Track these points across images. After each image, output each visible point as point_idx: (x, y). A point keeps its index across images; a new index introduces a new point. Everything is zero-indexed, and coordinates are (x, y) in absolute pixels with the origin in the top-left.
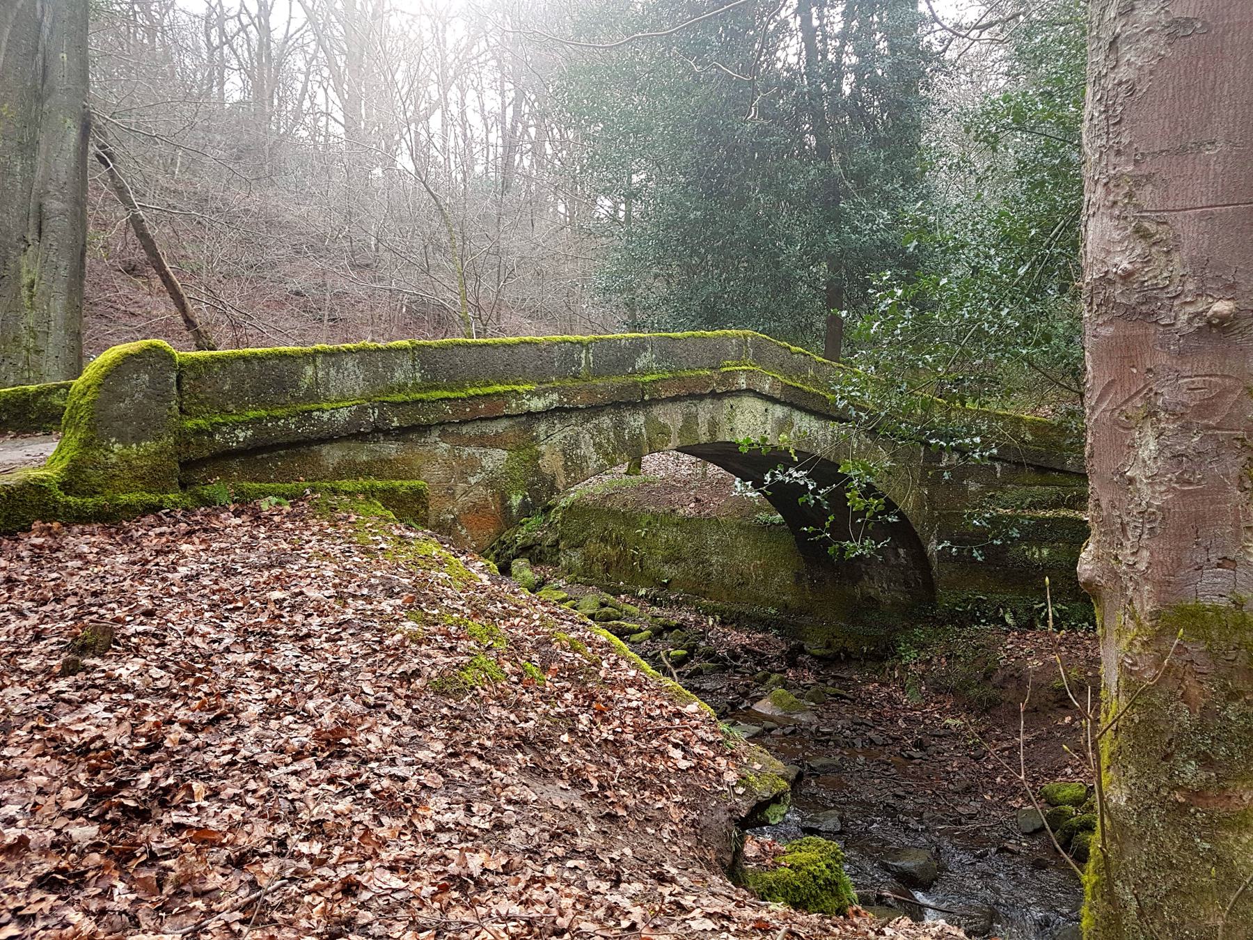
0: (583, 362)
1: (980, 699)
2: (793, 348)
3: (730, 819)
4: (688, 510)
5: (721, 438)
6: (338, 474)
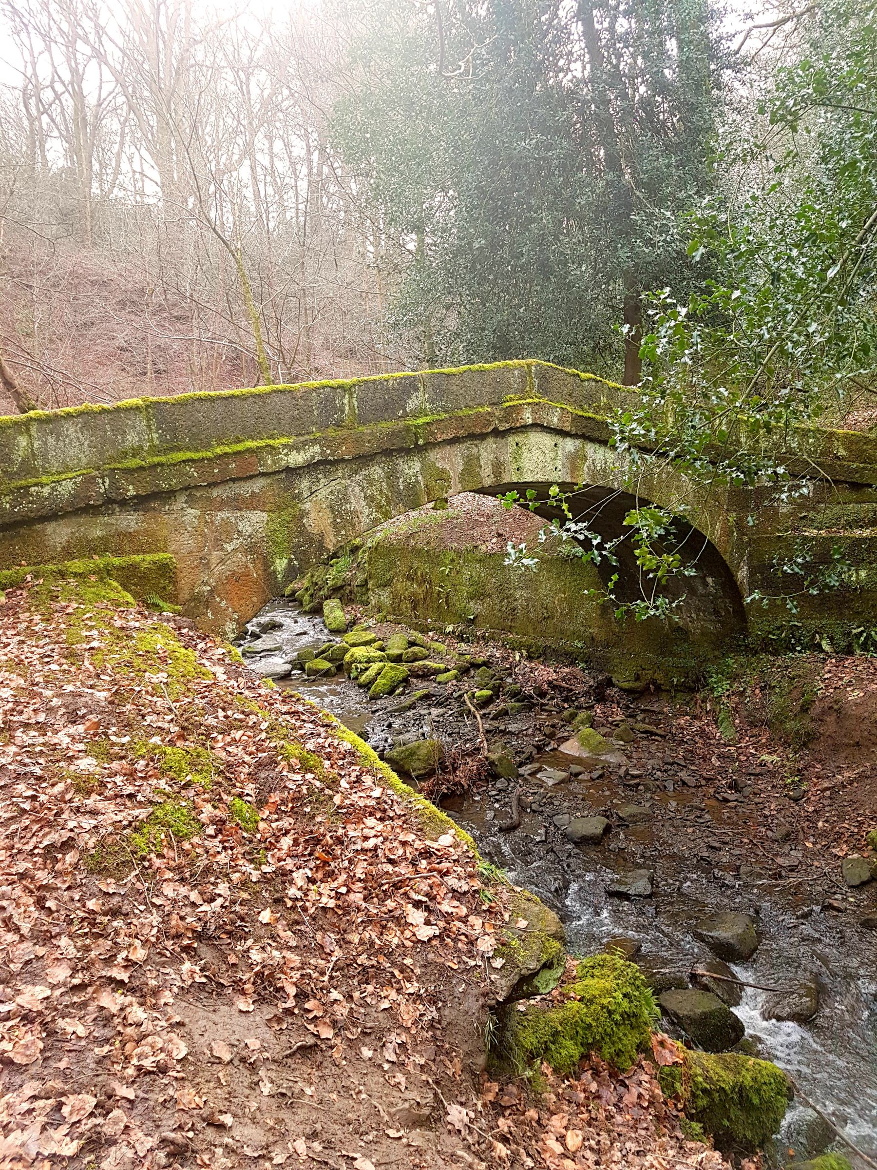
0: (347, 408)
1: (797, 732)
2: (583, 375)
3: (483, 1006)
4: (490, 545)
6: (68, 553)
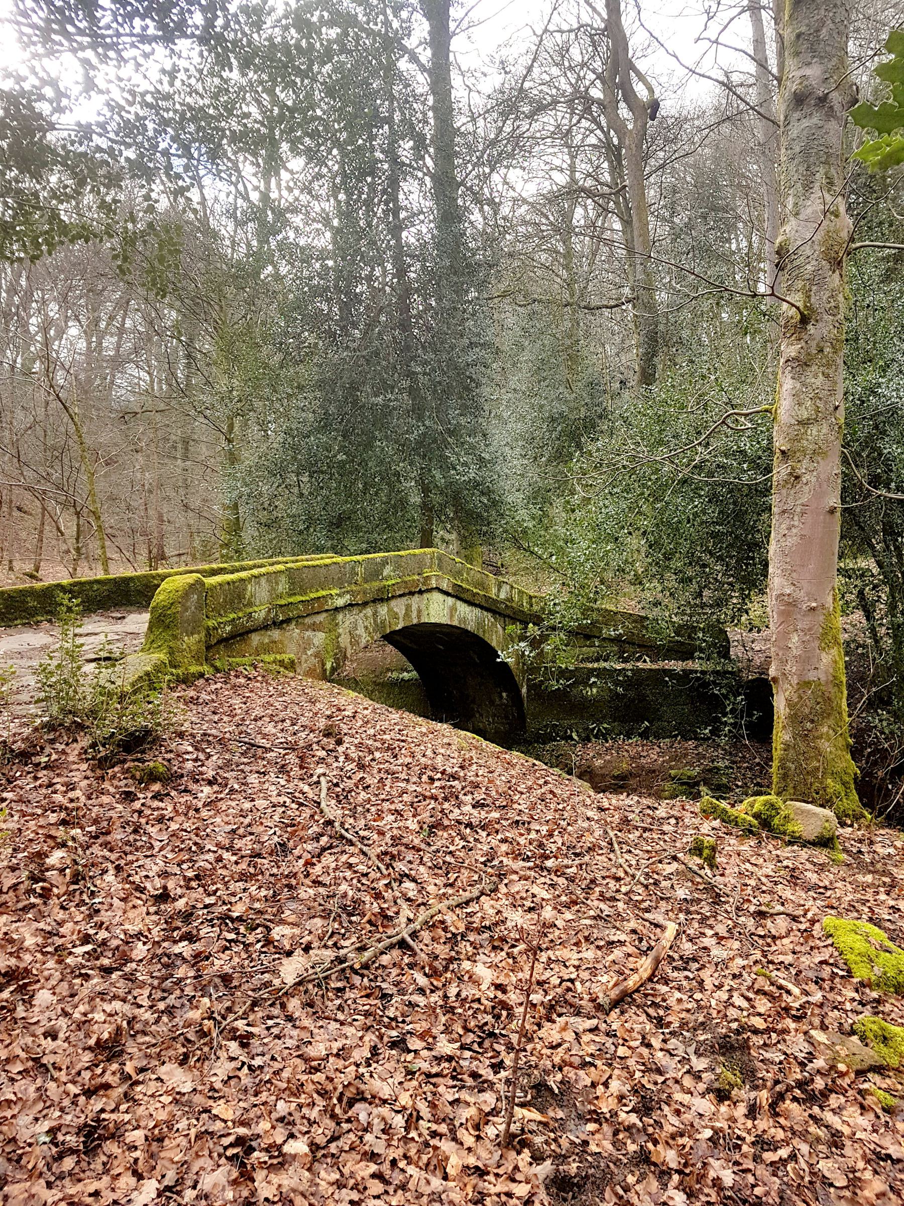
5: (425, 619)
